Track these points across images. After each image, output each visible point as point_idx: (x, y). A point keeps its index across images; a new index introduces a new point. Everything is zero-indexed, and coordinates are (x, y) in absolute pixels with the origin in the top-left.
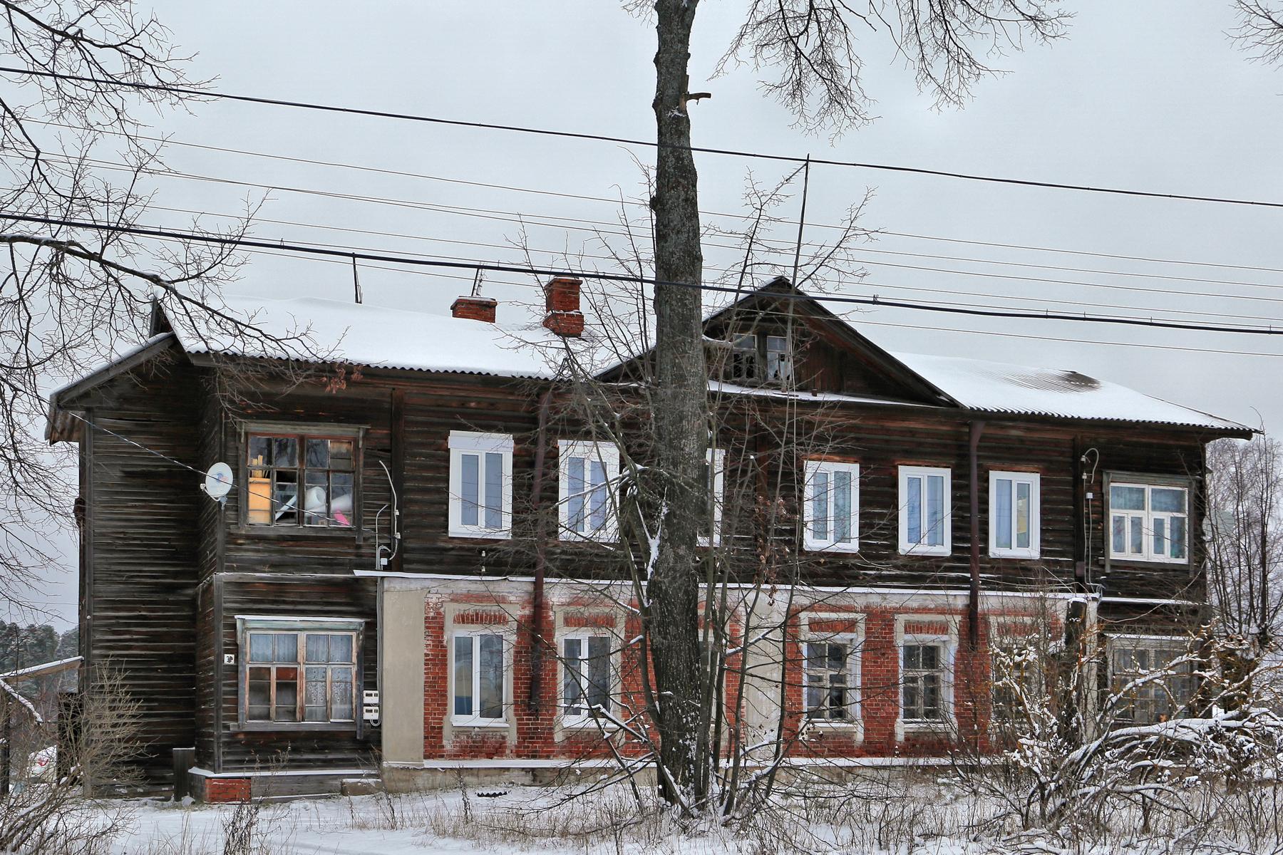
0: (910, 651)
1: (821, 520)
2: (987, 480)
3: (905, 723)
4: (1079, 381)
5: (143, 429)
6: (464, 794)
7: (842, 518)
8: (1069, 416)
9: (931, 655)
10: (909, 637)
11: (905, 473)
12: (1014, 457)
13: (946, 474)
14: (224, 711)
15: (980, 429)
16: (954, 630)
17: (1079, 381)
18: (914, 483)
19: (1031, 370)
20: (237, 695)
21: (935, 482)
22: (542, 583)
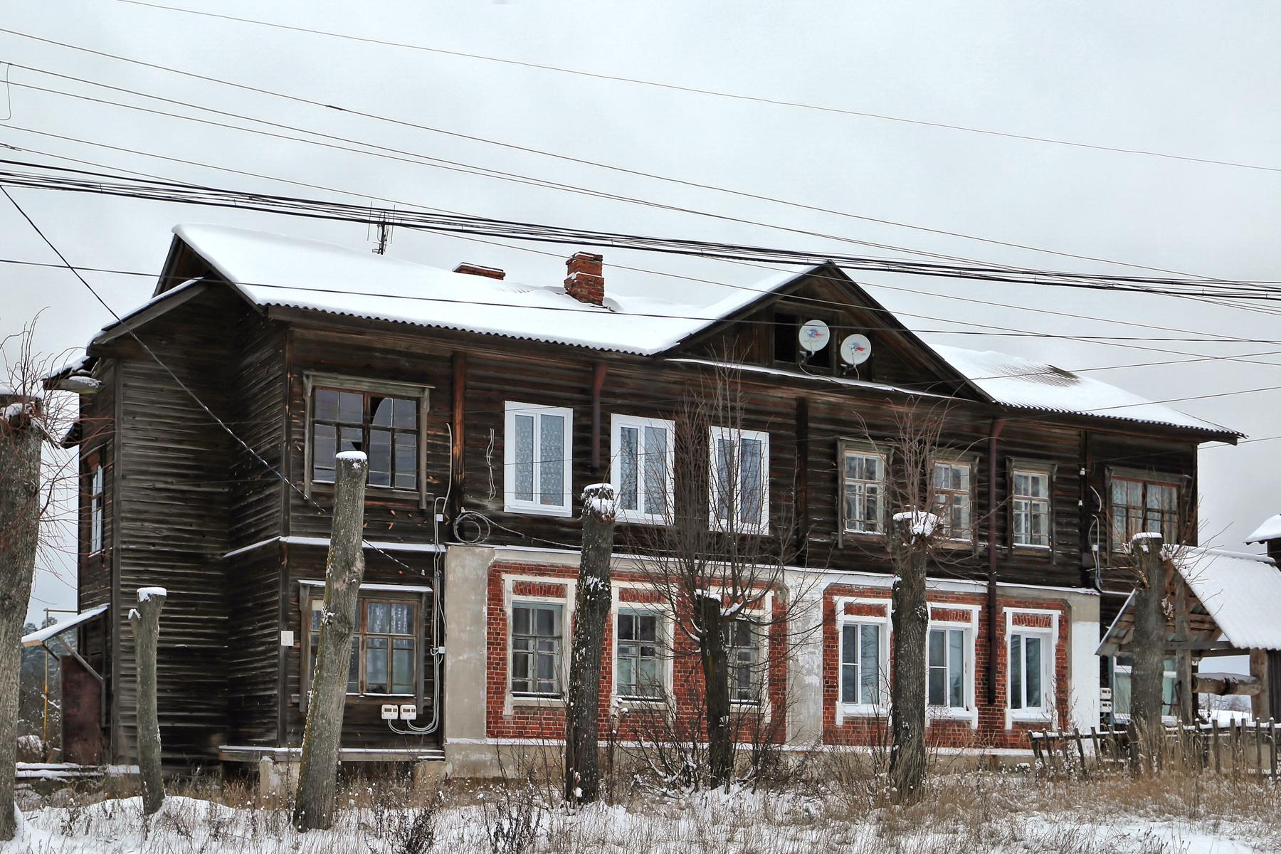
0: (625, 620)
1: (726, 500)
2: (706, 438)
3: (515, 695)
4: (1064, 376)
5: (178, 415)
6: (548, 786)
7: (750, 494)
8: (1084, 413)
9: (548, 618)
10: (625, 605)
11: (513, 410)
12: (1036, 452)
13: (567, 414)
14: (962, 724)
15: (1002, 422)
16: (975, 617)
17: (1064, 376)
18: (525, 424)
19: (1019, 361)
20: (299, 683)
21: (552, 425)
22: (920, 596)
